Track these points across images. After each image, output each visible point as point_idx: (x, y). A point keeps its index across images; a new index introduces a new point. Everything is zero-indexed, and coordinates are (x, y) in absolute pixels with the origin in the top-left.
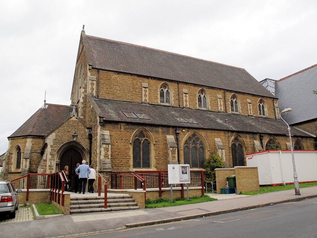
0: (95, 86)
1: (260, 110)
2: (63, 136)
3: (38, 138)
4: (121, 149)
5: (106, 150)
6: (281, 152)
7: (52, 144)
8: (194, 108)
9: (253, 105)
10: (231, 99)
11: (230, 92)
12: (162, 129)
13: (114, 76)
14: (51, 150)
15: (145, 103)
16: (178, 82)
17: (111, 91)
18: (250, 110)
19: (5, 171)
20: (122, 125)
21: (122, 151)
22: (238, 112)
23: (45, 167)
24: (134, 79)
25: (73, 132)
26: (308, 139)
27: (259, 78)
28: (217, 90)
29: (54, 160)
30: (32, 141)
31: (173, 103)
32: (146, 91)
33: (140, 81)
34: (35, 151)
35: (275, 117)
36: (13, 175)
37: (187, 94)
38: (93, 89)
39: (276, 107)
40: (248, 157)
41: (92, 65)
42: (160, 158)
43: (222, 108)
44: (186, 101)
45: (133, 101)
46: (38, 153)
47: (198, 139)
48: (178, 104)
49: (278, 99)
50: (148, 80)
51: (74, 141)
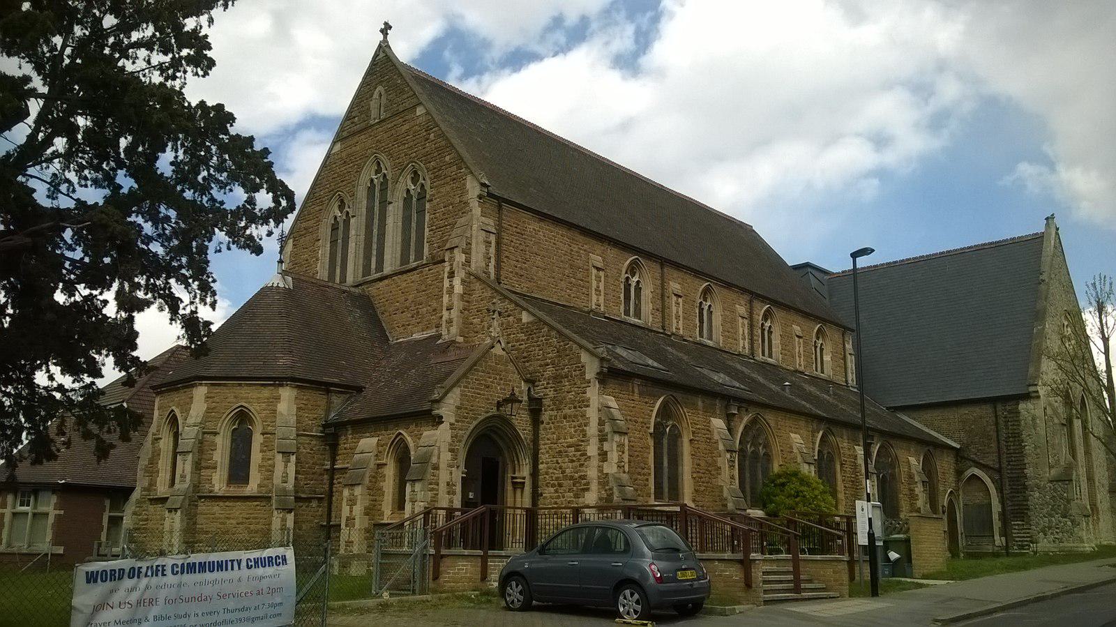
0: (492, 250)
1: (627, 298)
2: (476, 398)
3: (312, 389)
5: (621, 446)
7: (453, 421)
8: (691, 339)
11: (762, 302)
13: (533, 225)
15: (596, 314)
16: (664, 262)
19: (191, 489)
20: (637, 382)
22: (640, 319)
23: (436, 487)
26: (945, 451)
29: (458, 467)
30: (296, 398)
31: (651, 320)
35: (846, 381)
36: (221, 504)
41: (488, 186)
44: (677, 317)
46: (311, 436)
51: (499, 417)
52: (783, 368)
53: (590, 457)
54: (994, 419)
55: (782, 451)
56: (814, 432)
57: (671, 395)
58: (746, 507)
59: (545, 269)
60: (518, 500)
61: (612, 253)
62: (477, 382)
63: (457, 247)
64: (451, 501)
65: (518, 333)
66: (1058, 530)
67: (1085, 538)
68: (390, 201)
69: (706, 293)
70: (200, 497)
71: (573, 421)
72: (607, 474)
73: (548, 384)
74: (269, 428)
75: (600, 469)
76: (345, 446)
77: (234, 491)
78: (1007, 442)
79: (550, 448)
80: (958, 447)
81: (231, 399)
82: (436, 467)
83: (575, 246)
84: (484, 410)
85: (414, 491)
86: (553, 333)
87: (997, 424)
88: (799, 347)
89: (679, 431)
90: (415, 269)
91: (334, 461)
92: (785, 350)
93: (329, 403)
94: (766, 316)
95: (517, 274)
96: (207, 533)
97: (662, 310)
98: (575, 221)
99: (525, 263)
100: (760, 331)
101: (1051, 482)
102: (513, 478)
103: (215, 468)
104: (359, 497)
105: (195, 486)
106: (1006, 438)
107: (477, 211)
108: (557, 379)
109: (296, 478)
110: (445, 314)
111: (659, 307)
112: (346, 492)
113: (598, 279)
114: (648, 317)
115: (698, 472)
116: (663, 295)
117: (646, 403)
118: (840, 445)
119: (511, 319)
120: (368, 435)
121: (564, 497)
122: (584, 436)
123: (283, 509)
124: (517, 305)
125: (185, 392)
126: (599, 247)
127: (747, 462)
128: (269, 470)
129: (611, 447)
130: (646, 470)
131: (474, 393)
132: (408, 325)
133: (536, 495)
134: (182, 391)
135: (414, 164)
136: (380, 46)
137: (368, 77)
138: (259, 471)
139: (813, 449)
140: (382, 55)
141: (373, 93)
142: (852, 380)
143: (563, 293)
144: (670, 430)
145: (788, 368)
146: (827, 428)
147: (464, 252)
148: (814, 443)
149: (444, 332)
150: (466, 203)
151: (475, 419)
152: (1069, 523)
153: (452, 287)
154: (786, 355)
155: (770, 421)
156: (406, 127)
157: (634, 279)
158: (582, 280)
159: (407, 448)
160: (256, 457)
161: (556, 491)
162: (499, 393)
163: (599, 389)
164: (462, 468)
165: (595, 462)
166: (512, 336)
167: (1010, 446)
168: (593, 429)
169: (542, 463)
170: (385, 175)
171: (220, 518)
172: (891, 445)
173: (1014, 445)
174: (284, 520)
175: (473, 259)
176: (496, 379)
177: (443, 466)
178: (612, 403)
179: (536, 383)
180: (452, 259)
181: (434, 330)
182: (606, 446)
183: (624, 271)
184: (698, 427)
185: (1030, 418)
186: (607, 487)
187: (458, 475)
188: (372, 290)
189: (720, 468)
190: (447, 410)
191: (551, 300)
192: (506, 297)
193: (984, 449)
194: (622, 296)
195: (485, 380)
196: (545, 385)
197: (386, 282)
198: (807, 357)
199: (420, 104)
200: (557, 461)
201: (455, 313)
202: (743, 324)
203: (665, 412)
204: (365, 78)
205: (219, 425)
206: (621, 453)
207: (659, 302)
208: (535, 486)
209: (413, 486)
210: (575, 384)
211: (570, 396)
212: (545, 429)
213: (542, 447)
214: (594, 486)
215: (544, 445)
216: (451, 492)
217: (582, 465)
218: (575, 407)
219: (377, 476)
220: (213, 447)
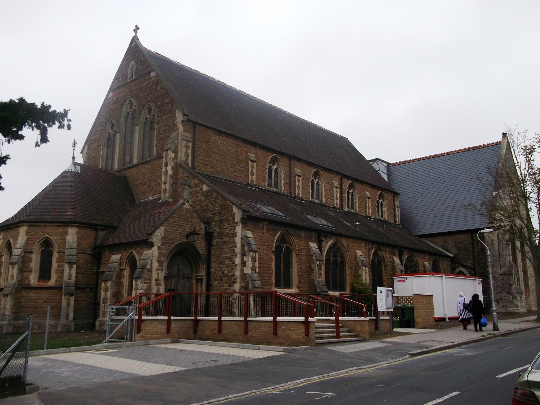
0: (190, 151)
1: (313, 189)
2: (174, 232)
4: (263, 260)
5: (253, 259)
6: (444, 276)
8: (307, 200)
9: (372, 201)
10: (269, 163)
11: (348, 179)
12: (305, 233)
13: (214, 137)
14: (159, 254)
16: (291, 158)
17: (210, 161)
18: (369, 209)
19: (17, 284)
21: (264, 262)
24: (238, 145)
25: (186, 227)
27: (368, 157)
28: (333, 174)
29: (162, 270)
30: (77, 233)
31: (283, 189)
32: (253, 167)
33: (246, 149)
34: (82, 250)
35: (395, 222)
36: (34, 291)
37: (255, 162)
38: (188, 155)
39: (397, 207)
40: (397, 280)
42: (303, 275)
43: (338, 203)
44: (299, 188)
45: (237, 181)
47: (338, 249)
48: (288, 191)
49: (399, 194)
50: (255, 150)
52: (359, 215)
53: (237, 264)
54: (471, 241)
55: (351, 259)
56: (369, 250)
57: (286, 230)
58: (327, 290)
59: (222, 161)
60: (199, 288)
61: (261, 153)
62: (174, 223)
63: (169, 149)
64: (158, 289)
65: (201, 196)
66: (505, 301)
67: (519, 305)
68: (137, 124)
69: (316, 175)
70: (23, 288)
71: (229, 245)
72: (246, 274)
73: (216, 224)
74: (62, 249)
75: (242, 271)
76: (105, 259)
77: (42, 284)
78: (478, 253)
79: (217, 260)
80: (452, 255)
81: (41, 233)
82: (150, 271)
83: (239, 149)
84: (179, 239)
85: (137, 284)
86: (219, 196)
87: (473, 244)
88: (369, 203)
89: (290, 250)
90: (149, 161)
91: (99, 268)
92: (361, 205)
93: (97, 235)
94: (350, 187)
95: (204, 164)
96: (26, 307)
97: (290, 184)
98: (239, 135)
99: (209, 158)
100: (346, 195)
101: (501, 275)
102: (196, 276)
103: (31, 271)
104: (110, 287)
105: (19, 281)
106: (477, 251)
107: (181, 129)
108: (221, 221)
109: (76, 277)
110: (163, 186)
111: (288, 181)
112: (103, 285)
113: (253, 167)
114: (283, 187)
115: (301, 272)
116: (290, 176)
117: (270, 234)
118: (385, 256)
119: (198, 189)
120: (116, 253)
121: (223, 286)
122: (234, 252)
123: (68, 294)
124: (201, 181)
125: (16, 230)
126: (253, 149)
127: (331, 267)
128: (61, 272)
129: (248, 260)
130: (270, 271)
131: (173, 229)
132: (145, 192)
133: (209, 286)
134: (14, 229)
135: (149, 103)
136: (133, 40)
137: (127, 56)
138: (56, 273)
139: (369, 258)
140: (134, 43)
141: (129, 65)
142: (398, 221)
143: (232, 175)
144: (285, 249)
145: (362, 215)
146: (378, 247)
147: (173, 152)
148: (369, 255)
149: (162, 196)
150: (176, 125)
151: (173, 244)
152: (511, 297)
153: (166, 171)
154: (361, 207)
155: (344, 244)
156: (146, 83)
157: (274, 167)
158: (243, 167)
159: (135, 260)
160: (55, 265)
161: (219, 283)
162: (187, 229)
163: (242, 227)
164: (165, 270)
165: (239, 268)
166: (198, 198)
167: (480, 256)
168: (238, 249)
169: (212, 268)
170: (135, 110)
171: (33, 299)
172: (414, 256)
173: (482, 255)
174: (69, 300)
175: (179, 155)
176: (186, 222)
177: (154, 270)
178: (250, 234)
179: (210, 224)
180: (167, 156)
181: (158, 195)
182: (245, 259)
183: (268, 163)
184: (301, 247)
185: (490, 241)
186: (245, 281)
187: (162, 275)
188: (128, 173)
189: (314, 269)
190: (157, 238)
191: (224, 178)
192: (195, 177)
193: (466, 257)
194: (267, 176)
195: (179, 223)
196: (215, 225)
197: (134, 168)
198: (373, 208)
199: (153, 70)
200: (220, 266)
201: (168, 186)
202: (337, 191)
203: (282, 240)
204: (125, 56)
205: (34, 248)
206: (253, 262)
207: (288, 179)
208: (208, 280)
209: (136, 281)
210: (230, 224)
211: (227, 231)
212: (214, 249)
213: (212, 259)
214: (238, 281)
215: (213, 258)
216: (158, 284)
217: (233, 269)
218: (229, 237)
219: (120, 276)
220: (30, 260)
